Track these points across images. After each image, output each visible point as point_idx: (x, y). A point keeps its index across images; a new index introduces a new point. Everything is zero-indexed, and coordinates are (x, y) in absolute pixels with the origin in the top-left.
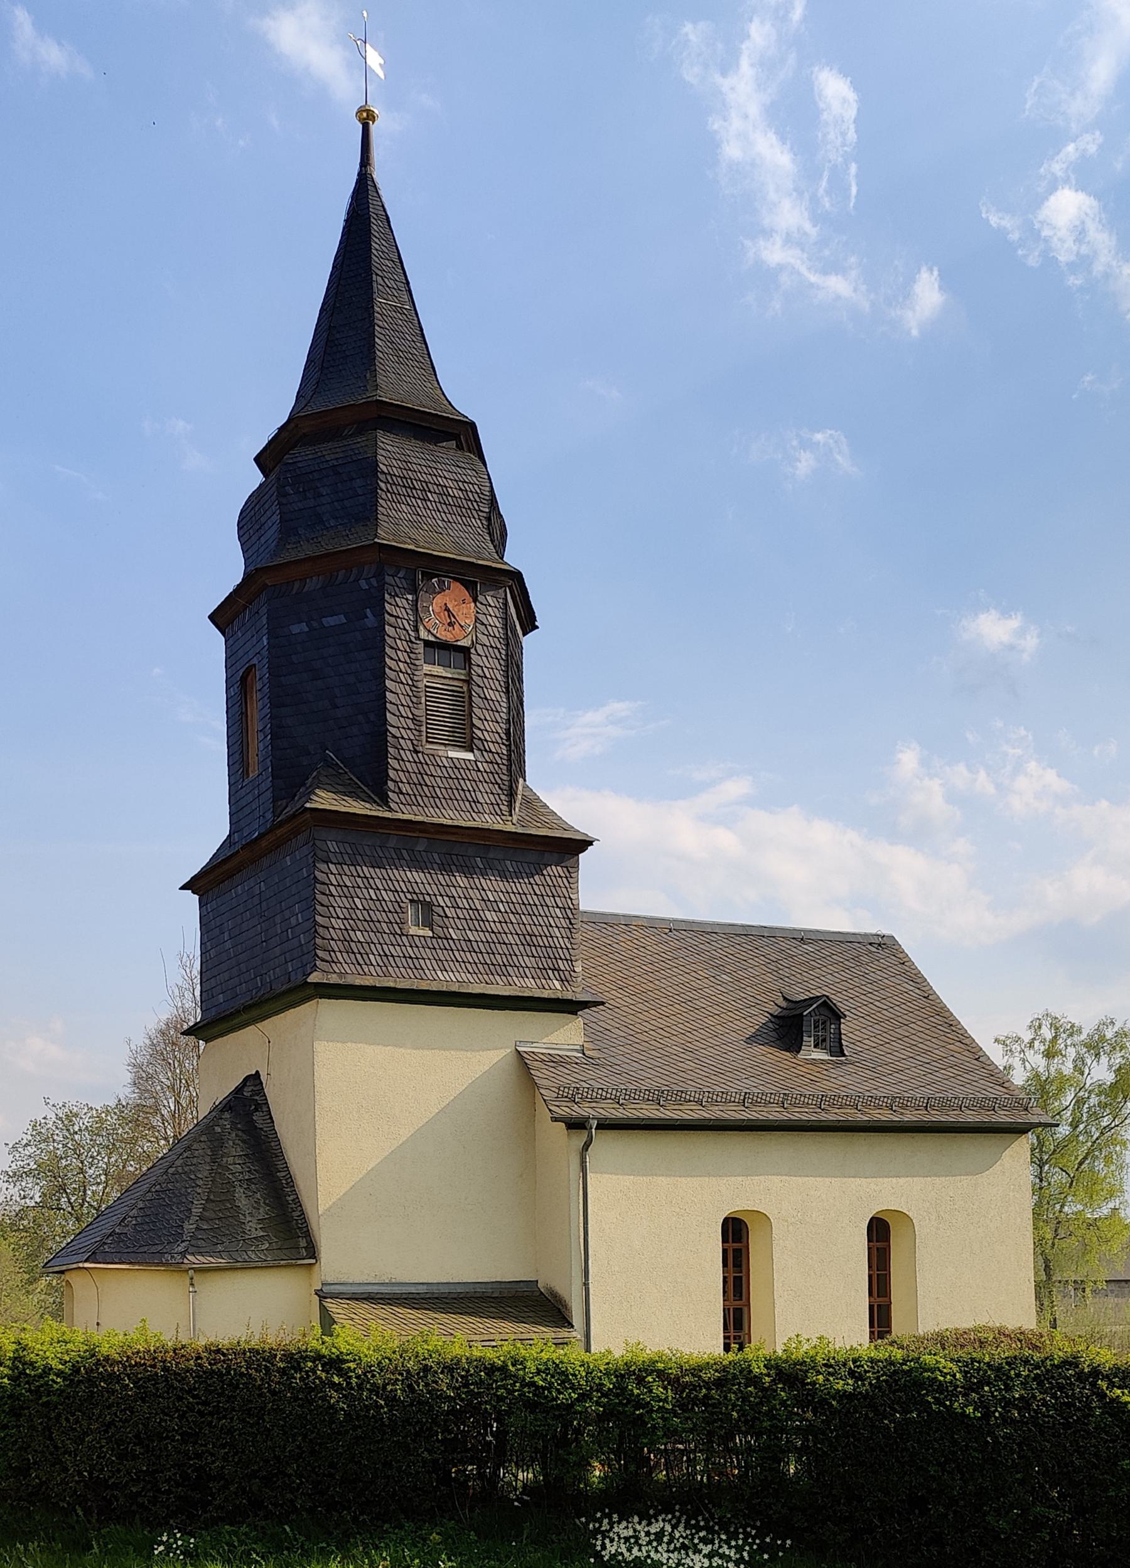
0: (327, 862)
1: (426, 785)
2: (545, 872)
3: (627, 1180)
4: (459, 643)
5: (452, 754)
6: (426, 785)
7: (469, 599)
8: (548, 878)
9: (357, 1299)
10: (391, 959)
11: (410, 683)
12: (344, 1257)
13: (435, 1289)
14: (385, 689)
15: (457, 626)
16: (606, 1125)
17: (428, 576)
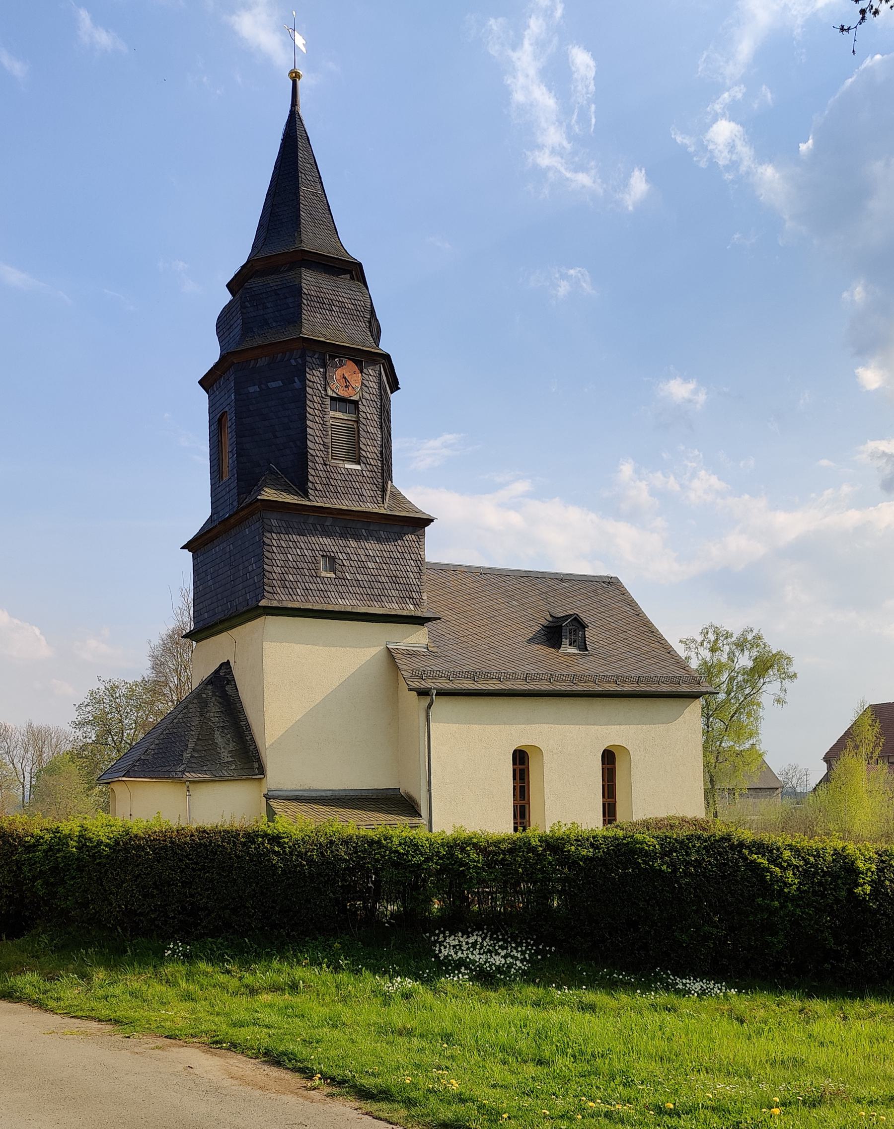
5: (347, 466)
7: (358, 371)
12: (284, 770)
13: (337, 794)
14: (307, 426)
15: (350, 388)
17: (333, 357)
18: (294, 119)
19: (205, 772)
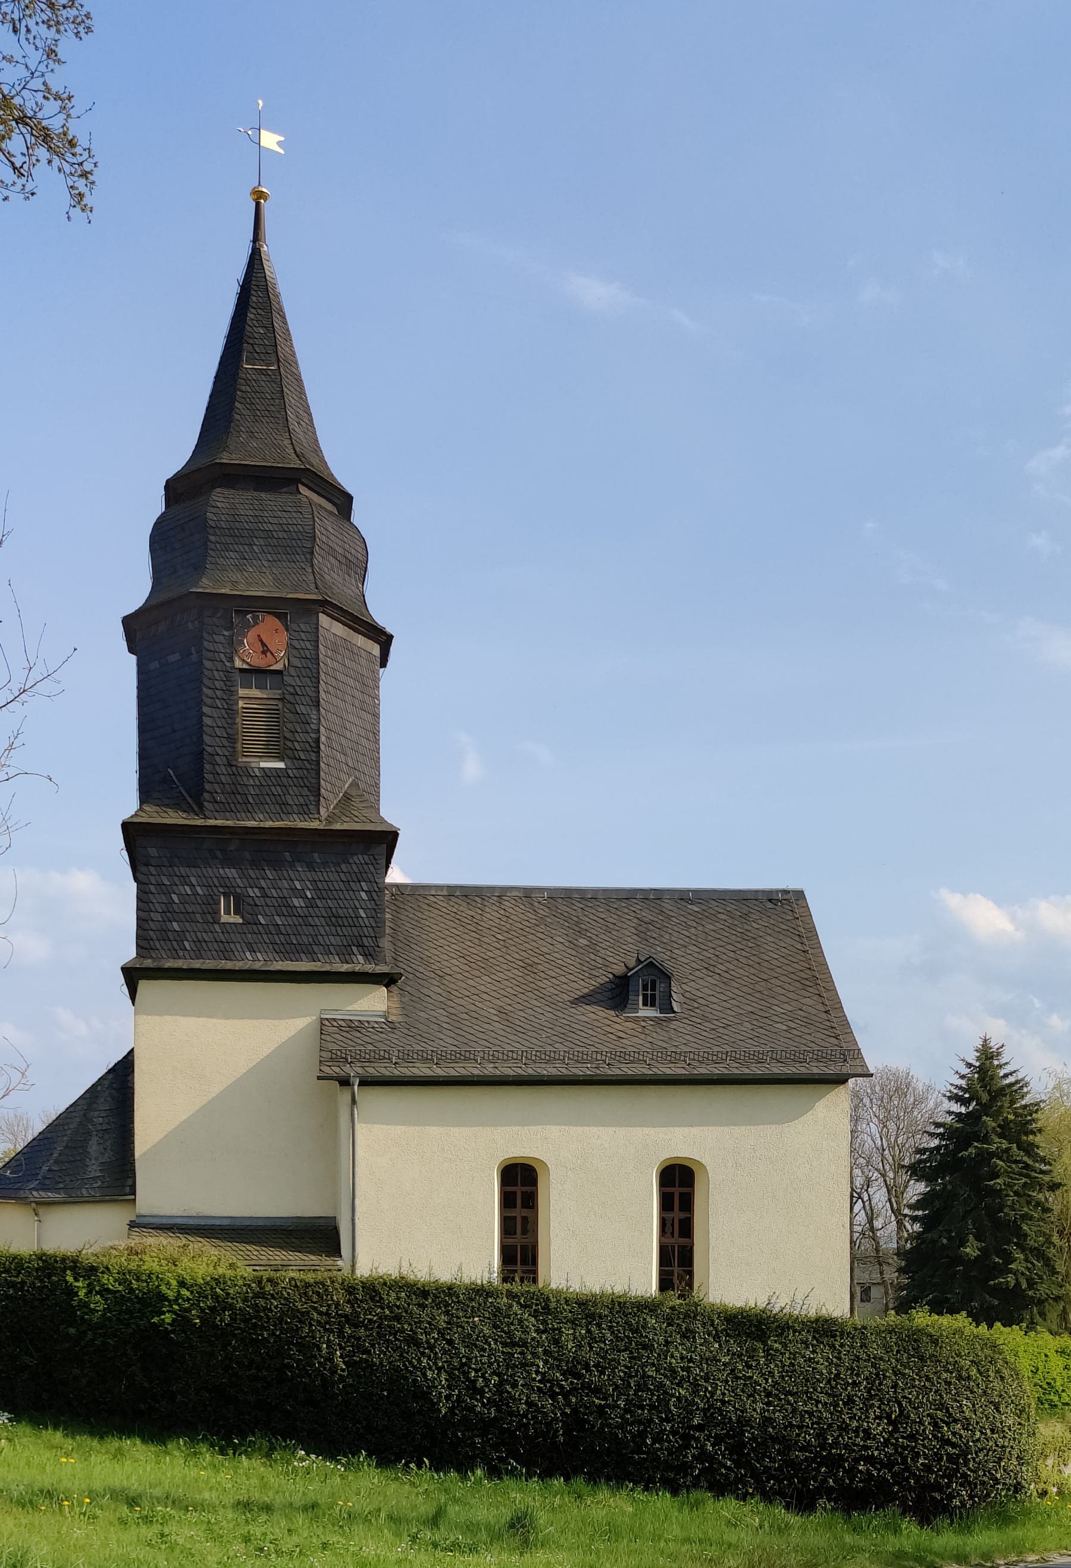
0: (147, 865)
3: (399, 1130)
4: (272, 668)
5: (263, 765)
7: (281, 628)
8: (354, 866)
9: (161, 1229)
10: (204, 944)
11: (226, 706)
12: (158, 1190)
13: (238, 1223)
14: (203, 714)
15: (268, 654)
16: (364, 1083)
18: (255, 260)
19: (57, 1190)
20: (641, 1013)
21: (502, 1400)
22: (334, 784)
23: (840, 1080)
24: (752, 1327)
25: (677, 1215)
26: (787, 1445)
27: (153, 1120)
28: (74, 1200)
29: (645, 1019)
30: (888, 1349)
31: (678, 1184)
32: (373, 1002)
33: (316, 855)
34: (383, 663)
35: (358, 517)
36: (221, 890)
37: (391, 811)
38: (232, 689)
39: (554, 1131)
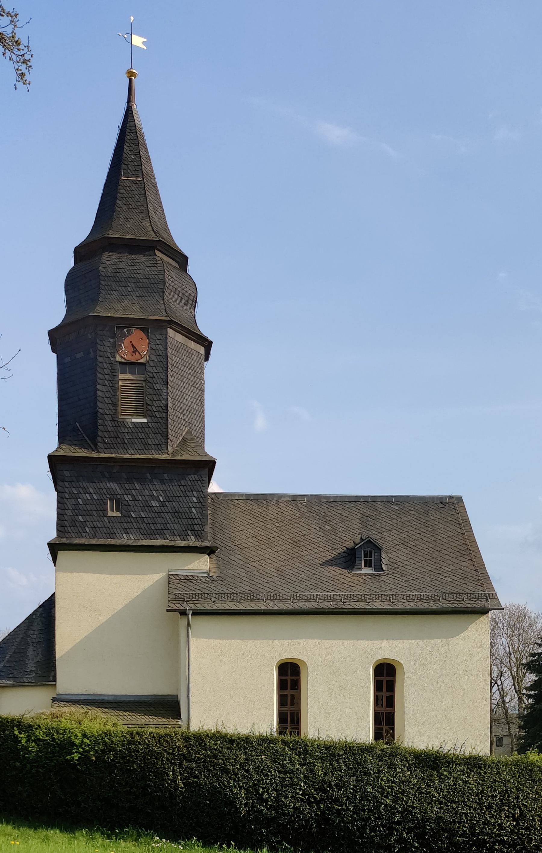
1: (119, 438)
2: (187, 479)
4: (139, 361)
5: (134, 420)
6: (119, 438)
9: (71, 702)
11: (111, 385)
12: (68, 681)
13: (118, 699)
15: (137, 353)
16: (195, 614)
17: (121, 328)
18: (129, 114)
19: (8, 679)
20: (363, 571)
21: (278, 807)
22: (176, 432)
23: (484, 612)
24: (431, 762)
25: (385, 693)
26: (452, 834)
27: (68, 635)
28: (19, 684)
29: (365, 575)
30: (513, 775)
31: (386, 676)
32: (200, 564)
33: (166, 475)
34: (207, 359)
35: (191, 270)
36: (108, 496)
37: (211, 448)
38: (115, 374)
39: (310, 643)
